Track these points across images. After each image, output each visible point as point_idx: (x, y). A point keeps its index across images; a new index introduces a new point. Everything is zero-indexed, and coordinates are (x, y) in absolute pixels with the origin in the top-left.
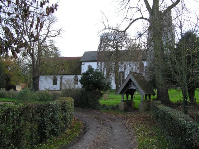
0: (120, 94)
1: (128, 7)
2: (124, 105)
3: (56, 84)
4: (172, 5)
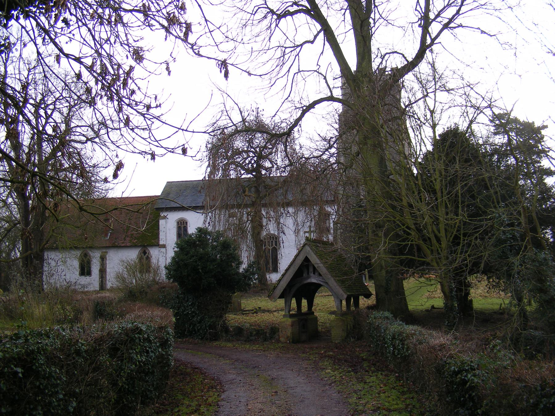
0: (281, 297)
1: (294, 69)
2: (292, 326)
3: (89, 273)
4: (403, 68)
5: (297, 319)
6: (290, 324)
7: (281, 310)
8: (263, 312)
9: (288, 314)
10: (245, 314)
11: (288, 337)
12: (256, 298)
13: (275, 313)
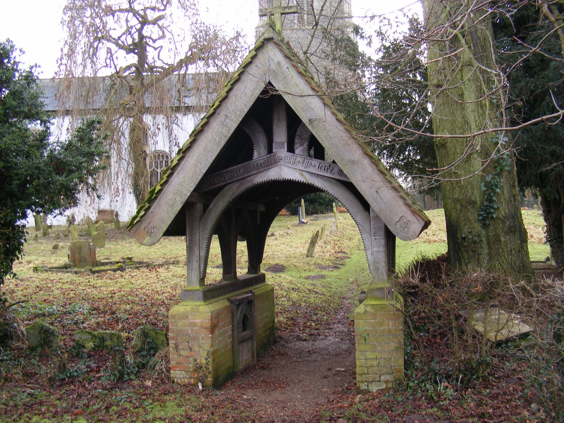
2: (213, 328)
5: (227, 303)
6: (208, 323)
7: (173, 263)
8: (137, 268)
9: (197, 287)
10: (98, 272)
11: (198, 368)
12: (131, 240)
13: (160, 270)
